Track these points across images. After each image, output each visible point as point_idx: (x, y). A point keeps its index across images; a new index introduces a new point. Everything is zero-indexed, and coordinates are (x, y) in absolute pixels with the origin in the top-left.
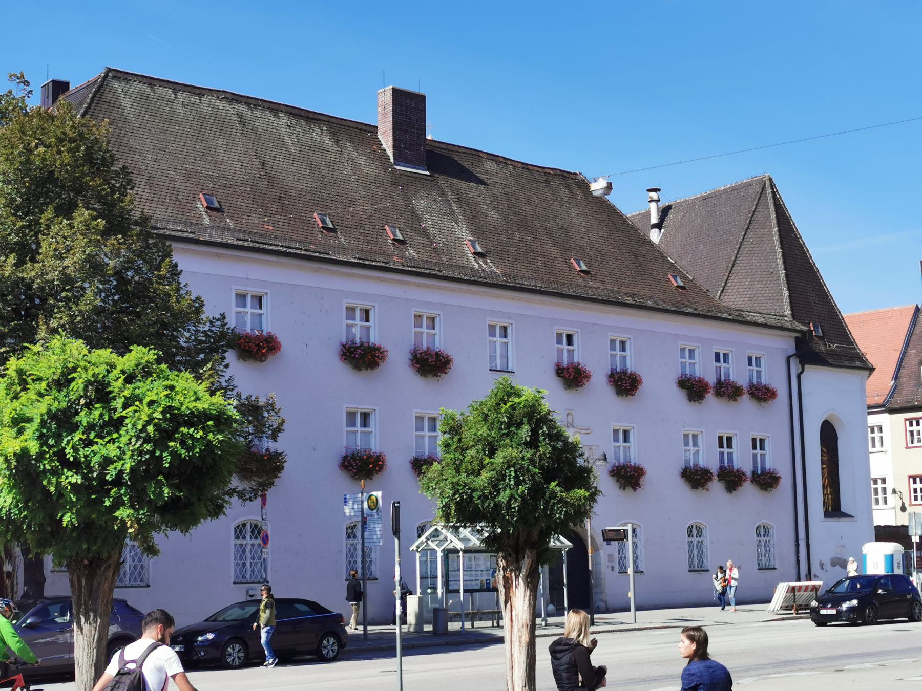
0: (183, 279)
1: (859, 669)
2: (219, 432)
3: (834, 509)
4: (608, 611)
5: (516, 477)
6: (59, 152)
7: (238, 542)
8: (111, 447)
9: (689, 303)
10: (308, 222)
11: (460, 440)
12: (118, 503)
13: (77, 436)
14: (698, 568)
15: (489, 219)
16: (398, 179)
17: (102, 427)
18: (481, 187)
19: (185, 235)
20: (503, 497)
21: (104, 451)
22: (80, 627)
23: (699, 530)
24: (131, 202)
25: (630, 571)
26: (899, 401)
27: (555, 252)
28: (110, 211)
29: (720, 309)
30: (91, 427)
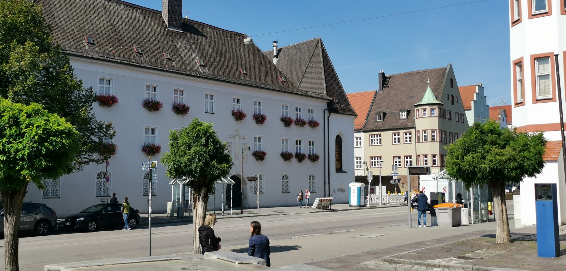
0: (74, 72)
1: (339, 233)
2: (68, 139)
3: (339, 169)
4: (249, 208)
5: (199, 158)
6: (19, 17)
7: (98, 180)
8: (20, 145)
9: (286, 88)
10: (130, 50)
11: (177, 143)
12: (22, 168)
13: (5, 140)
14: (285, 192)
15: (207, 51)
16: (169, 33)
17: (16, 136)
18: (204, 38)
19: (78, 54)
20: (193, 167)
21: (16, 146)
22: (7, 219)
23: (287, 177)
24: (51, 39)
25: (258, 193)
26: (368, 127)
27: (233, 65)
28: (42, 43)
29: (298, 90)
30: (11, 136)
